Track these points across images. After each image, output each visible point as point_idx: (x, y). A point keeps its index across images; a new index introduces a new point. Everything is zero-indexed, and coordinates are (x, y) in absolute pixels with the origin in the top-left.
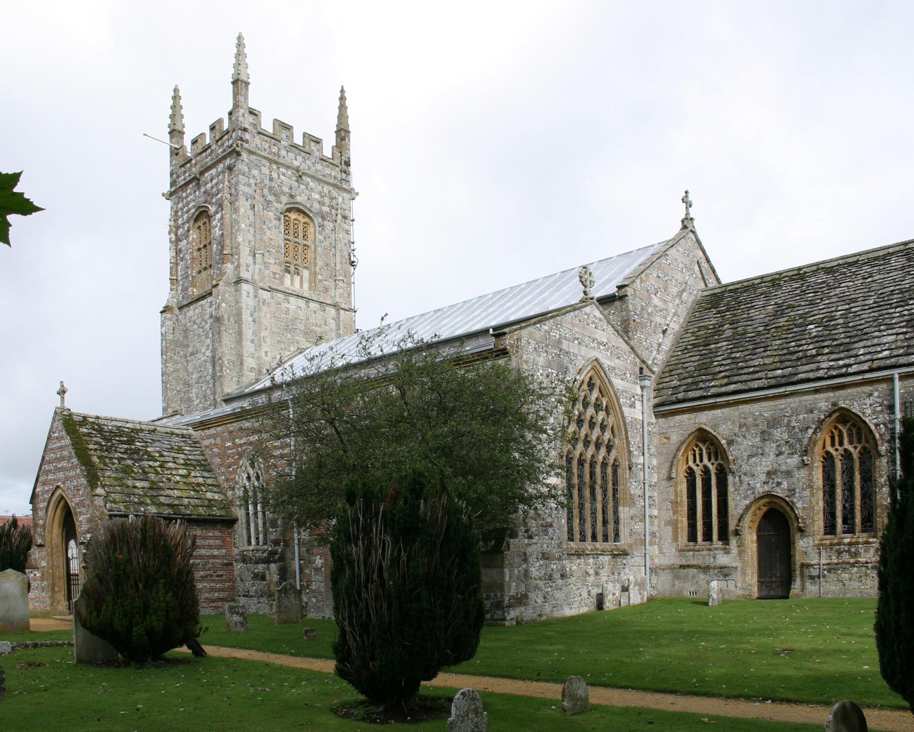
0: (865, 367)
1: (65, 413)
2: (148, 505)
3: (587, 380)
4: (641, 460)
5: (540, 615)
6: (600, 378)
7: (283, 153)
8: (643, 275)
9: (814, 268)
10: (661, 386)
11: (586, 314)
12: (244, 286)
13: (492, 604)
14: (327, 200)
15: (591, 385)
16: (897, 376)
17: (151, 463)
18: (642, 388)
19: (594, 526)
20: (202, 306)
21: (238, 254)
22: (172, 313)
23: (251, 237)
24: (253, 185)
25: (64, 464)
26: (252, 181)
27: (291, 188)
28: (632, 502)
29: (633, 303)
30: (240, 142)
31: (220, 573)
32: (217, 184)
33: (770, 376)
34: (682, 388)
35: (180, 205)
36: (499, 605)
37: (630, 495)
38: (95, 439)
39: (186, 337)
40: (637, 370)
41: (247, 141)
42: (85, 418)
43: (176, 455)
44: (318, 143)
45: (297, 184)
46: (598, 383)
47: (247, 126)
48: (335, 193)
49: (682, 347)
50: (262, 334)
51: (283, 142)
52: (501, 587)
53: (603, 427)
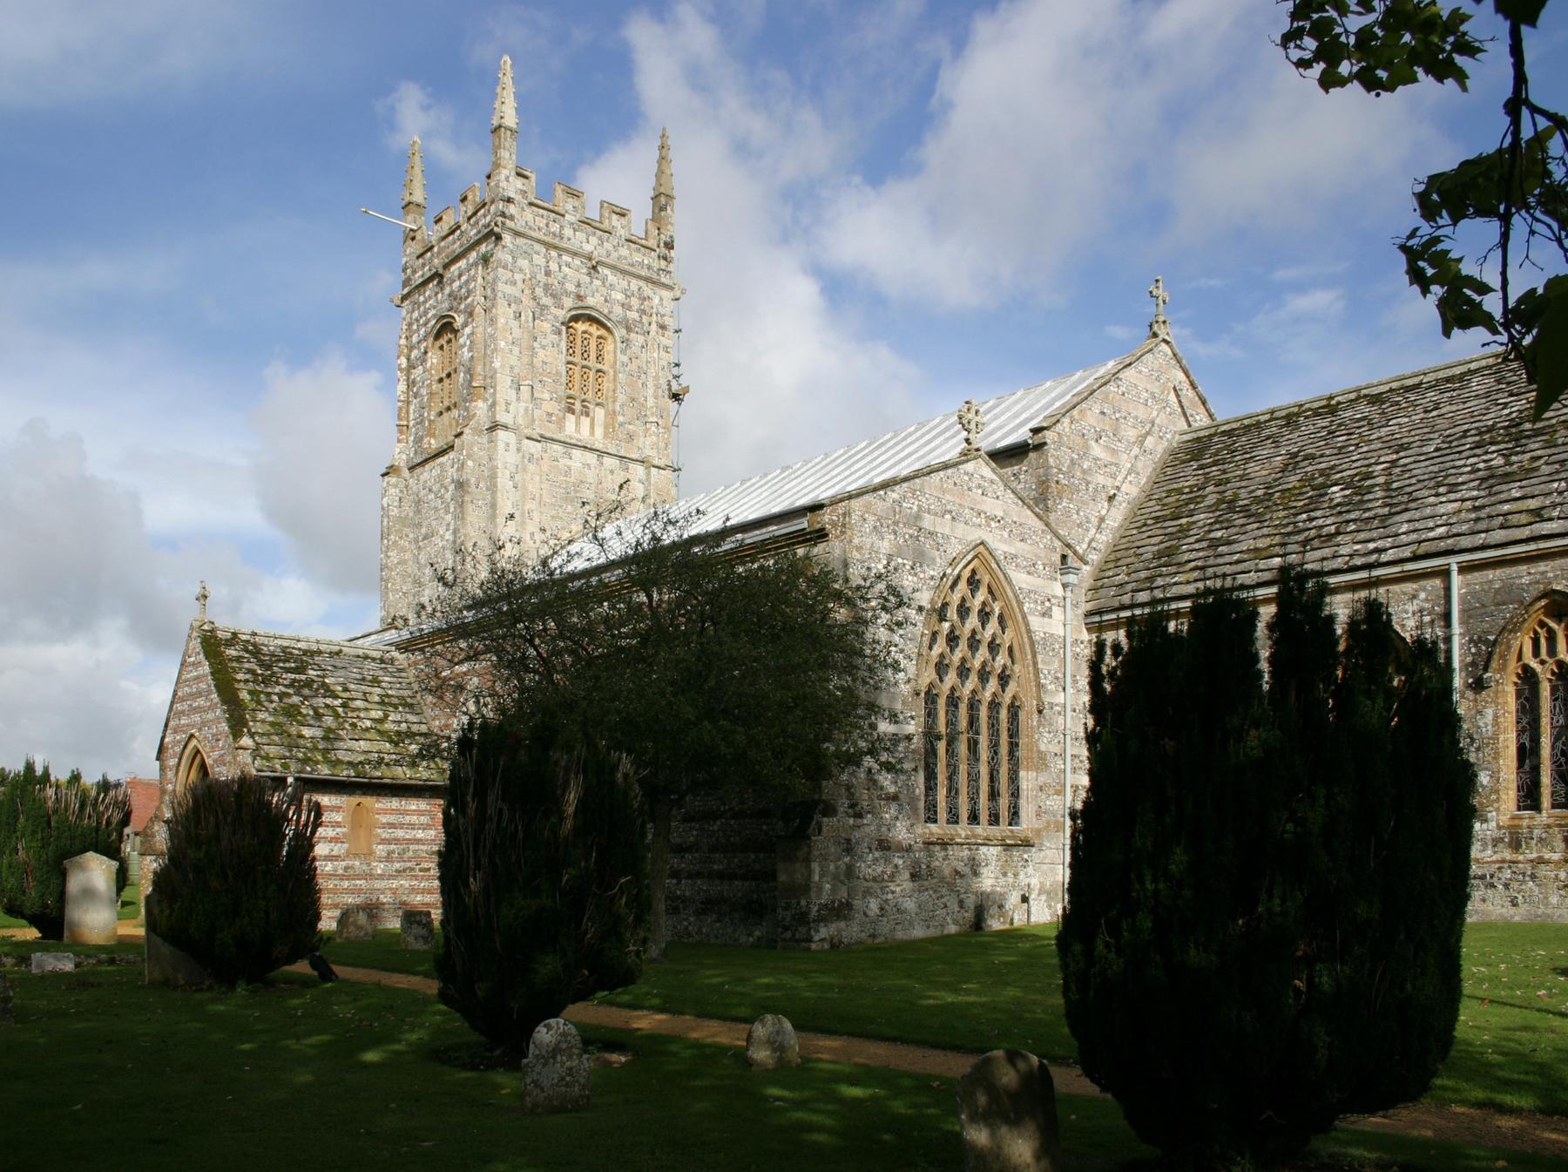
0: (1407, 553)
1: (206, 627)
2: (317, 763)
3: (966, 574)
4: (1060, 698)
5: (873, 936)
6: (991, 572)
7: (568, 232)
8: (1075, 412)
9: (1353, 396)
10: (1100, 583)
11: (966, 473)
12: (501, 434)
13: (793, 917)
14: (635, 302)
15: (973, 583)
16: (1455, 567)
17: (329, 701)
18: (1065, 586)
19: (973, 799)
20: (441, 465)
21: (494, 387)
22: (399, 476)
23: (513, 361)
24: (520, 283)
25: (201, 702)
26: (518, 277)
27: (579, 285)
28: (1042, 762)
29: (1057, 455)
30: (500, 219)
31: (425, 865)
32: (467, 282)
33: (1261, 567)
34: (1129, 587)
35: (416, 314)
36: (803, 918)
37: (1039, 752)
38: (247, 665)
39: (418, 512)
40: (1057, 558)
41: (512, 218)
42: (235, 634)
43: (369, 689)
44: (623, 215)
45: (588, 279)
46: (986, 579)
47: (512, 195)
48: (648, 290)
49: (1139, 522)
50: (527, 507)
51: (568, 217)
52: (805, 889)
53: (993, 647)
